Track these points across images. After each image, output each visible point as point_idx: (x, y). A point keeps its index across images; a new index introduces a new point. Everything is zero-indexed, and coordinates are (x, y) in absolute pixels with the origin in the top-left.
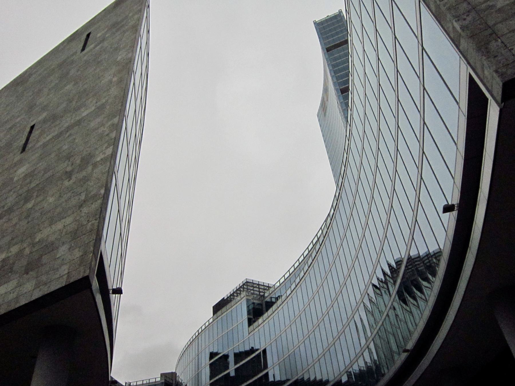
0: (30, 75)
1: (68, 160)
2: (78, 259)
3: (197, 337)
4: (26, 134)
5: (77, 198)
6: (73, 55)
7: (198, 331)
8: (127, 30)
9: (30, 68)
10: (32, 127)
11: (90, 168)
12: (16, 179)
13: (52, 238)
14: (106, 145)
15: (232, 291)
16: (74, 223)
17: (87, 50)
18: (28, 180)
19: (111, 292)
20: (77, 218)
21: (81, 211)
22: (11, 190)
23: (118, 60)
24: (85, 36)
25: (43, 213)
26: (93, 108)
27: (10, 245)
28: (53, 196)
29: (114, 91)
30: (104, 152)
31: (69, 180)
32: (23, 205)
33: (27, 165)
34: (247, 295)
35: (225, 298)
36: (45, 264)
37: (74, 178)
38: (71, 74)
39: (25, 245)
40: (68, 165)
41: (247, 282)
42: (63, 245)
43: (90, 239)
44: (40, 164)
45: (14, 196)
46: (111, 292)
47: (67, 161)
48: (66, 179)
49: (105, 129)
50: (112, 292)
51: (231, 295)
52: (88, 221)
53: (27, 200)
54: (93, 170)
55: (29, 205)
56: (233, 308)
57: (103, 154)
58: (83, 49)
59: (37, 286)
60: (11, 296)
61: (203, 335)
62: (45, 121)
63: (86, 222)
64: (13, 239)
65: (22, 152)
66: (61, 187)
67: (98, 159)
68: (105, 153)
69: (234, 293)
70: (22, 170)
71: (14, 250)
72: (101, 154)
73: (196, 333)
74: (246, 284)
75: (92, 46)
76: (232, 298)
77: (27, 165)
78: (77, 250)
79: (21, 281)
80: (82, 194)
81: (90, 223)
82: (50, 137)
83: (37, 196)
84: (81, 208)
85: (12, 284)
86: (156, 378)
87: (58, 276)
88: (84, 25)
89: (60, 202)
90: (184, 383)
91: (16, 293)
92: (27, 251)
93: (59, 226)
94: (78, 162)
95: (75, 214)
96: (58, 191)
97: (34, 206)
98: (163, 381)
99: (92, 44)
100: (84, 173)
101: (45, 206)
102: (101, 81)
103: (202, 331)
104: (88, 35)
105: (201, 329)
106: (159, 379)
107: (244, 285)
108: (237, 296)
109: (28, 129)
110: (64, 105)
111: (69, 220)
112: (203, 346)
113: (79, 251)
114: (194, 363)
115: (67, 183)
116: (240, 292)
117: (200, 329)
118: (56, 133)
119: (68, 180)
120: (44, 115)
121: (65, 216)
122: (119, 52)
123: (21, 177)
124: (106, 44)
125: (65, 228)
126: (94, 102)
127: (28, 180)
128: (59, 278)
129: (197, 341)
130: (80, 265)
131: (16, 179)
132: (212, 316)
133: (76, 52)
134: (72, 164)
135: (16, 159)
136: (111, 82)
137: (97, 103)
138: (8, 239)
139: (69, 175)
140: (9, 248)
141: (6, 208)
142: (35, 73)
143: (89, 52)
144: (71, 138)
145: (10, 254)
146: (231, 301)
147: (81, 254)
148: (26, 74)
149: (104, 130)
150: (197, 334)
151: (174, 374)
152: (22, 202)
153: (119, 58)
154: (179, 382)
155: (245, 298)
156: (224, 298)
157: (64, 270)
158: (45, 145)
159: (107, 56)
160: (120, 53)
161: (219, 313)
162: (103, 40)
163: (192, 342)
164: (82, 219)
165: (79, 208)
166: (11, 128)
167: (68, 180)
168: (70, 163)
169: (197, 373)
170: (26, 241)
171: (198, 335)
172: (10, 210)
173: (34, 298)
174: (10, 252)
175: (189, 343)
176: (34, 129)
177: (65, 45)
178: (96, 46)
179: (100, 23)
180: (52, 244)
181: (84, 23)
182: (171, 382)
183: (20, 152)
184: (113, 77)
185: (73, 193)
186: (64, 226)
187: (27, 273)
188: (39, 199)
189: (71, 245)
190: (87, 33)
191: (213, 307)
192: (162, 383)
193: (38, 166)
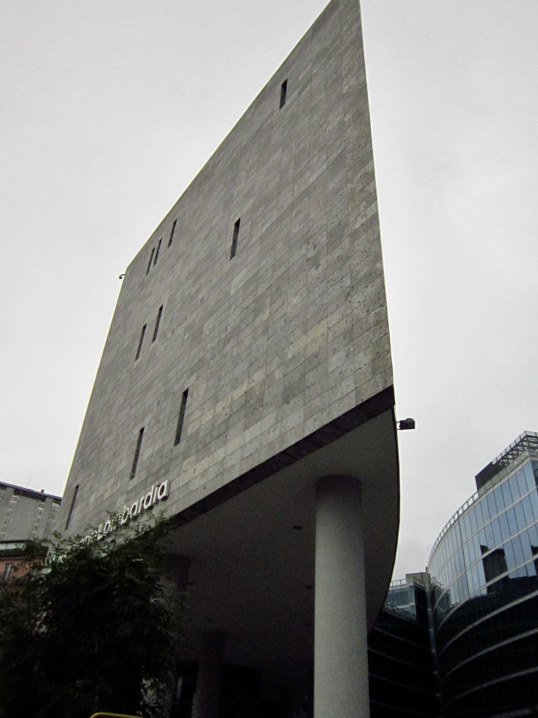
1: (306, 244)
2: (366, 366)
3: (457, 522)
5: (338, 286)
7: (458, 512)
8: (345, 51)
10: (237, 224)
11: (346, 242)
12: (232, 292)
13: (313, 349)
14: (364, 203)
16: (345, 320)
17: (287, 103)
18: (252, 287)
19: (398, 425)
20: (348, 312)
21: (350, 301)
22: (230, 307)
23: (344, 92)
24: (279, 87)
25: (287, 321)
26: (325, 166)
27: (249, 373)
28: (296, 295)
29: (352, 133)
31: (317, 268)
33: (244, 271)
34: (531, 456)
35: (494, 463)
36: (313, 385)
37: (323, 263)
38: (273, 142)
39: (273, 368)
40: (308, 250)
41: (527, 436)
42: (334, 353)
44: (264, 262)
45: (238, 312)
46: (398, 425)
47: (305, 245)
48: (313, 266)
50: (400, 427)
51: (503, 458)
52: (367, 311)
53: (257, 311)
54: (352, 243)
55: (264, 317)
56: (503, 481)
57: (362, 218)
59: (308, 415)
60: (272, 436)
61: (467, 517)
62: (254, 209)
63: (365, 313)
64: (251, 365)
65: (231, 258)
67: (357, 226)
68: (366, 215)
70: (239, 279)
71: (258, 377)
72: (359, 218)
74: (520, 444)
75: (296, 93)
77: (244, 271)
78: (361, 354)
80: (343, 279)
81: (372, 314)
82: (268, 224)
83: (272, 302)
84: (350, 297)
85: (269, 420)
86: (401, 580)
87: (339, 396)
89: (312, 299)
90: (445, 589)
91: (277, 432)
92: (278, 375)
94: (324, 240)
95: (342, 308)
96: (303, 286)
98: (412, 584)
99: (295, 90)
100: (338, 252)
101: (288, 310)
103: (464, 512)
104: (284, 86)
105: (461, 509)
107: (522, 441)
108: (514, 459)
109: (233, 228)
110: (277, 179)
111: (333, 319)
112: (469, 535)
113: (366, 355)
114: (453, 562)
115: (314, 272)
116: (518, 453)
117: (460, 509)
118: (274, 219)
119: (314, 267)
120: (251, 202)
121: (325, 314)
123: (239, 286)
124: (315, 83)
125: (331, 331)
126: (325, 157)
127: (252, 287)
128: (342, 398)
129: (457, 527)
130: (374, 373)
131: (232, 292)
132: (476, 490)
134: (315, 247)
135: (226, 269)
136: (342, 123)
137: (327, 158)
138: (244, 366)
140: (249, 377)
141: (229, 330)
143: (291, 105)
144: (301, 216)
145: (254, 384)
146: (504, 466)
147: (369, 357)
148: (208, 167)
150: (456, 517)
151: (424, 576)
152: (251, 316)
153: (344, 88)
154: (437, 586)
155: (528, 459)
156: (491, 463)
157: (347, 386)
158: (262, 239)
159: (323, 96)
160: (344, 83)
161: (488, 484)
162: (310, 79)
166: (207, 237)
168: (310, 246)
170: (273, 362)
171: (458, 519)
172: (237, 331)
173: (308, 433)
175: (442, 535)
176: (240, 225)
177: (252, 111)
178: (300, 94)
179: (297, 63)
180: (316, 356)
182: (423, 585)
183: (229, 258)
186: (329, 328)
187: (288, 403)
188: (275, 306)
189: (349, 349)
191: (477, 477)
192: (411, 587)
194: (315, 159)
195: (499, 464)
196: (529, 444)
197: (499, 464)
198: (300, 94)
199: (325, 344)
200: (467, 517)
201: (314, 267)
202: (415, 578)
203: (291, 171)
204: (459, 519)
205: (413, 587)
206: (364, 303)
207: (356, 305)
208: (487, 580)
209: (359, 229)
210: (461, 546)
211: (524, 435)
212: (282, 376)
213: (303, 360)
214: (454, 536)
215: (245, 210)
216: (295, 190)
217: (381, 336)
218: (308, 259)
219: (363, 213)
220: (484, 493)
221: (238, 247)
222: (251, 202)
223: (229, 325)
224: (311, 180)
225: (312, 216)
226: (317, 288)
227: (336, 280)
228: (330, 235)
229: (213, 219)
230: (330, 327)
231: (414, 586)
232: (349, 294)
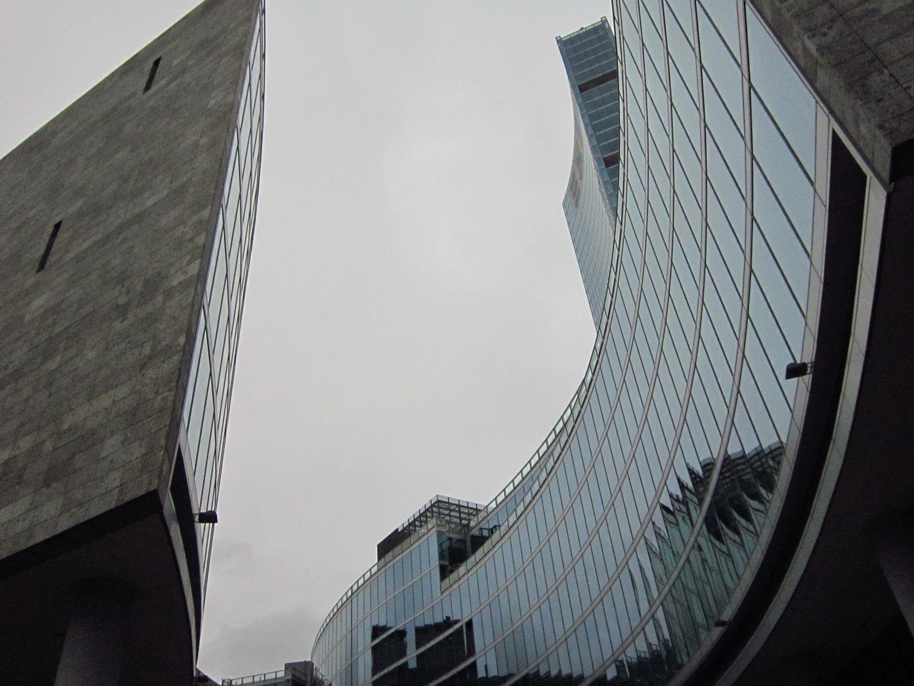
0: (54, 133)
3: (350, 599)
4: (46, 237)
5: (136, 352)
7: (352, 588)
10: (57, 226)
12: (27, 318)
14: (188, 257)
16: (132, 396)
17: (154, 88)
18: (50, 321)
19: (197, 518)
20: (138, 388)
21: (143, 375)
22: (19, 338)
23: (209, 106)
24: (150, 64)
26: (165, 192)
29: (203, 162)
31: (123, 321)
32: (42, 364)
34: (438, 525)
36: (80, 469)
37: (130, 316)
38: (126, 132)
39: (45, 436)
40: (120, 294)
41: (438, 501)
44: (72, 292)
46: (197, 518)
50: (199, 519)
51: (410, 524)
52: (156, 393)
53: (48, 355)
55: (52, 365)
60: (20, 527)
62: (80, 215)
63: (153, 394)
64: (22, 425)
65: (38, 271)
67: (175, 283)
68: (186, 272)
69: (415, 520)
70: (39, 303)
71: (26, 444)
75: (164, 81)
78: (137, 444)
79: (38, 499)
81: (160, 397)
83: (66, 349)
85: (22, 505)
86: (276, 672)
87: (102, 490)
92: (48, 446)
93: (105, 401)
94: (139, 287)
97: (60, 366)
98: (290, 677)
99: (164, 77)
103: (358, 588)
104: (157, 63)
108: (421, 526)
109: (50, 230)
111: (122, 391)
113: (140, 446)
114: (343, 646)
115: (118, 326)
118: (100, 236)
119: (120, 319)
120: (79, 203)
124: (187, 78)
126: (168, 180)
129: (349, 606)
131: (27, 318)
133: (135, 93)
135: (29, 283)
136: (196, 145)
137: (171, 182)
139: (122, 311)
141: (10, 370)
143: (157, 92)
145: (18, 452)
146: (410, 535)
147: (144, 451)
151: (308, 665)
152: (39, 360)
154: (319, 678)
155: (435, 529)
156: (397, 529)
157: (114, 480)
158: (79, 258)
160: (213, 95)
161: (389, 556)
163: (340, 607)
164: (146, 388)
166: (19, 228)
171: (351, 596)
172: (18, 374)
173: (60, 530)
174: (18, 448)
178: (170, 82)
183: (35, 269)
186: (114, 402)
187: (48, 486)
190: (155, 59)
191: (379, 546)
192: (288, 680)
193: (67, 294)
194: (160, 177)
195: (405, 531)
196: (439, 511)
197: (405, 531)
198: (170, 82)
199: (105, 421)
200: (368, 590)
201: (120, 319)
202: (295, 669)
203: (131, 183)
204: (354, 594)
205: (291, 681)
206: (156, 381)
207: (148, 381)
208: (374, 674)
209: (175, 287)
210: (350, 630)
211: (436, 500)
212: (51, 449)
213: (79, 434)
214: (344, 619)
215: (72, 209)
216: (129, 209)
217: (161, 427)
218: (118, 306)
219: (184, 269)
220: (384, 566)
221: (50, 258)
222: (79, 203)
223: (11, 362)
224: (149, 203)
225: (136, 250)
226: (116, 347)
227: (137, 342)
228: (147, 283)
229: (33, 207)
230: (116, 401)
231: (293, 680)
232: (145, 365)
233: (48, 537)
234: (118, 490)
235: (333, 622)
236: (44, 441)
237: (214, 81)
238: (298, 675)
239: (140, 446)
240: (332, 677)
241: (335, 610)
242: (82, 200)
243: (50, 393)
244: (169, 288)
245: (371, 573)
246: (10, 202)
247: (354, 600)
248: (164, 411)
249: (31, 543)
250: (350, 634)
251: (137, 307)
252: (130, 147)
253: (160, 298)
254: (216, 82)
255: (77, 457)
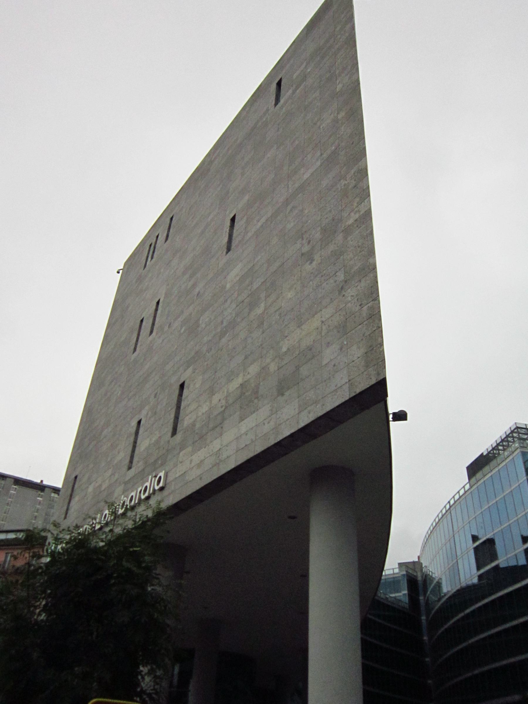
0: (211, 162)
3: (449, 511)
4: (227, 229)
5: (332, 281)
6: (265, 114)
7: (449, 502)
9: (208, 155)
10: (233, 220)
12: (228, 286)
14: (358, 199)
15: (490, 447)
16: (338, 314)
17: (282, 101)
19: (391, 417)
20: (341, 306)
21: (344, 296)
22: (226, 301)
23: (338, 90)
24: (274, 86)
26: (319, 163)
30: (356, 209)
31: (311, 263)
32: (249, 313)
34: (521, 447)
35: (484, 454)
36: (307, 377)
37: (317, 258)
39: (268, 360)
40: (303, 245)
41: (517, 428)
42: (328, 346)
43: (373, 327)
44: (259, 257)
45: (234, 306)
46: (391, 417)
48: (307, 261)
49: (348, 181)
51: (493, 449)
52: (360, 305)
53: (253, 305)
55: (259, 311)
58: (276, 104)
59: (302, 408)
60: (267, 428)
61: (458, 508)
64: (246, 358)
65: (227, 253)
66: (301, 275)
69: (498, 445)
71: (253, 369)
73: (446, 505)
75: (290, 91)
76: (496, 454)
77: (240, 266)
78: (355, 347)
79: (276, 405)
82: (263, 220)
83: (267, 297)
84: (343, 291)
85: (264, 412)
86: (393, 569)
87: (333, 388)
88: (317, 11)
90: (437, 577)
91: (272, 423)
92: (273, 367)
93: (315, 322)
94: (318, 236)
97: (266, 309)
98: (405, 573)
99: (289, 89)
100: (332, 247)
101: (283, 304)
102: (319, 127)
103: (455, 502)
104: (279, 84)
106: (396, 571)
107: (512, 432)
108: (504, 450)
109: (228, 223)
111: (327, 313)
115: (308, 267)
117: (451, 499)
118: (269, 214)
119: (309, 262)
120: (247, 198)
121: (319, 308)
122: (336, 80)
125: (325, 325)
126: (319, 154)
128: (336, 391)
129: (449, 516)
130: (367, 366)
131: (228, 286)
132: (467, 480)
133: (268, 110)
136: (336, 121)
137: (321, 155)
138: (239, 359)
139: (309, 257)
141: (225, 324)
142: (215, 158)
145: (249, 376)
146: (495, 457)
147: (363, 350)
149: (346, 182)
151: (416, 565)
154: (429, 575)
155: (518, 451)
156: (482, 454)
157: (341, 379)
160: (338, 81)
161: (479, 475)
162: (304, 77)
163: (441, 518)
164: (349, 305)
165: (340, 292)
166: (203, 232)
167: (309, 262)
168: (304, 241)
169: (455, 561)
171: (449, 509)
172: (233, 324)
173: (302, 424)
174: (248, 374)
181: (317, 10)
184: (338, 114)
185: (322, 276)
186: (323, 322)
187: (283, 395)
189: (343, 342)
190: (277, 81)
191: (468, 468)
192: (403, 575)
193: (256, 260)
194: (309, 156)
199: (319, 337)
200: (458, 508)
204: (450, 509)
208: (478, 568)
209: (352, 225)
211: (515, 427)
212: (276, 368)
216: (290, 186)
222: (247, 198)
224: (306, 176)
227: (329, 274)
228: (324, 230)
229: (209, 214)
232: (342, 288)
233: (293, 431)
234: (347, 385)
235: (436, 530)
236: (269, 364)
237: (336, 72)
238: (411, 572)
239: (359, 348)
240: (441, 572)
241: (434, 524)
242: (248, 195)
243: (263, 330)
244: (346, 227)
245: (459, 494)
246: (191, 218)
247: (453, 512)
248: (373, 317)
249: (280, 438)
250: (453, 539)
251: (321, 250)
252: (275, 147)
253: (340, 237)
254: (337, 72)
255: (301, 369)
